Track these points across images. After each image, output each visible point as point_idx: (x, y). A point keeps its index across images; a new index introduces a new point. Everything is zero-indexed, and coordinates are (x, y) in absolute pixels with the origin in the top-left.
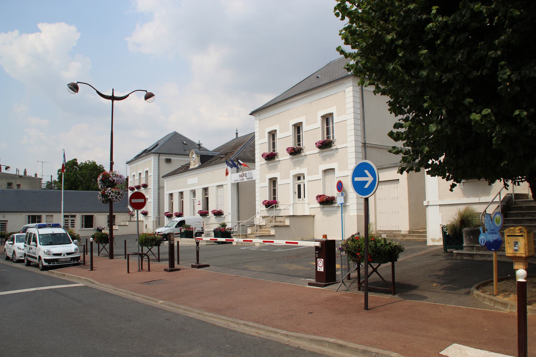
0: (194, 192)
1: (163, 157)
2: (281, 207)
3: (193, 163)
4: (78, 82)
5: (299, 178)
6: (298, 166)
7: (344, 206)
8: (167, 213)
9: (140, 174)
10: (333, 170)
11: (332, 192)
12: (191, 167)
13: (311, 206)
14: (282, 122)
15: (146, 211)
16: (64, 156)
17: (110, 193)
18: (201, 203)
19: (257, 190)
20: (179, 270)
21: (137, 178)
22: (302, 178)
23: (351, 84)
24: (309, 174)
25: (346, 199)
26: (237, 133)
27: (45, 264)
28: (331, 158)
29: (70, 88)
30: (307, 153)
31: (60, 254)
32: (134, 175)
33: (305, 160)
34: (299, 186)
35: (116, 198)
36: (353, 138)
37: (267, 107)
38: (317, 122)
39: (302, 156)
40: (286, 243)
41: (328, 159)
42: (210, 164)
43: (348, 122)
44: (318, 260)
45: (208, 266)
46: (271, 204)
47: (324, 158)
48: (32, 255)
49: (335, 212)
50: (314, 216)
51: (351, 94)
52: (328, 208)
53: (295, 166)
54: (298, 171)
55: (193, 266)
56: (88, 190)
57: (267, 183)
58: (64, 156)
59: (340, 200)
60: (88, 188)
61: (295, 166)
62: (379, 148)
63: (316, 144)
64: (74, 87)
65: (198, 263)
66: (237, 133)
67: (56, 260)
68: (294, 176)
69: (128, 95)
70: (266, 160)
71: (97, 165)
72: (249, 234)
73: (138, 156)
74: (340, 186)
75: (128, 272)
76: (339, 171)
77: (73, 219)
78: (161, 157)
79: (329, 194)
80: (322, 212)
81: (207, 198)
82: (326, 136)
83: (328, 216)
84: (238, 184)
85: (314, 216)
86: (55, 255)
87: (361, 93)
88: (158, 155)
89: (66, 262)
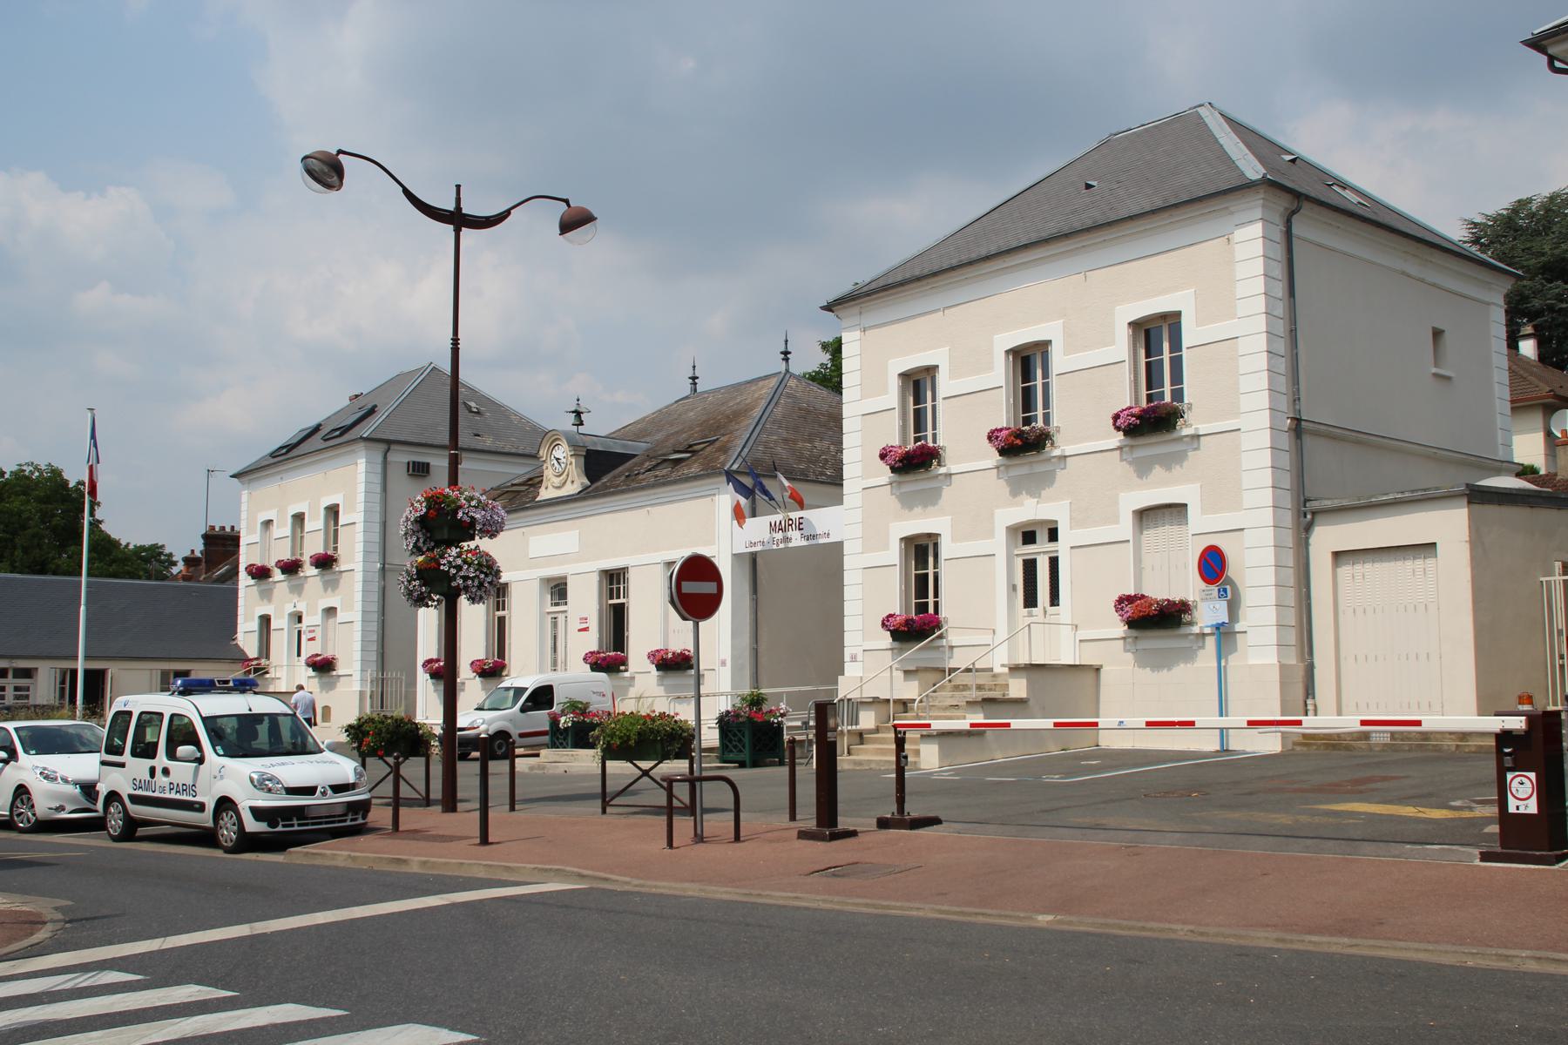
0: (558, 590)
1: (401, 457)
2: (953, 638)
3: (557, 481)
4: (340, 152)
5: (1029, 537)
6: (1032, 494)
7: (1225, 634)
8: (430, 661)
9: (299, 518)
10: (1177, 510)
11: (1184, 584)
12: (545, 494)
13: (1082, 634)
14: (965, 345)
15: (328, 654)
16: (93, 436)
17: (459, 568)
18: (593, 624)
19: (850, 577)
20: (853, 834)
21: (283, 529)
22: (1042, 536)
23: (1258, 213)
24: (1076, 523)
25: (1233, 608)
26: (694, 378)
27: (252, 825)
28: (1169, 469)
29: (310, 172)
30: (1069, 450)
31: (310, 791)
32: (268, 523)
33: (1059, 473)
34: (1030, 567)
35: (481, 585)
36: (1263, 400)
37: (868, 294)
38: (1113, 343)
39: (1049, 459)
40: (1364, 723)
41: (1158, 471)
42: (632, 484)
43: (1243, 346)
44: (1509, 776)
45: (935, 821)
46: (915, 628)
47: (1142, 469)
48: (173, 796)
49: (1188, 655)
50: (1098, 670)
51: (1258, 247)
52: (1157, 641)
53: (1015, 493)
54: (1029, 510)
55: (883, 824)
56: (42, 572)
57: (893, 554)
58: (93, 436)
59: (1207, 613)
60: (41, 568)
61: (1015, 493)
62: (1334, 438)
63: (1116, 417)
64: (326, 171)
65: (901, 809)
66: (694, 378)
67: (299, 812)
68: (1012, 530)
69: (507, 213)
70: (893, 469)
71: (66, 483)
72: (870, 732)
73: (289, 448)
74: (1213, 565)
75: (670, 844)
76: (1204, 511)
77: (22, 682)
78: (392, 457)
79: (1159, 590)
80: (1130, 656)
81: (502, 620)
82: (1144, 393)
83: (1156, 667)
84: (754, 558)
85: (1098, 670)
86: (292, 791)
87: (1284, 245)
88: (383, 447)
89: (330, 818)
